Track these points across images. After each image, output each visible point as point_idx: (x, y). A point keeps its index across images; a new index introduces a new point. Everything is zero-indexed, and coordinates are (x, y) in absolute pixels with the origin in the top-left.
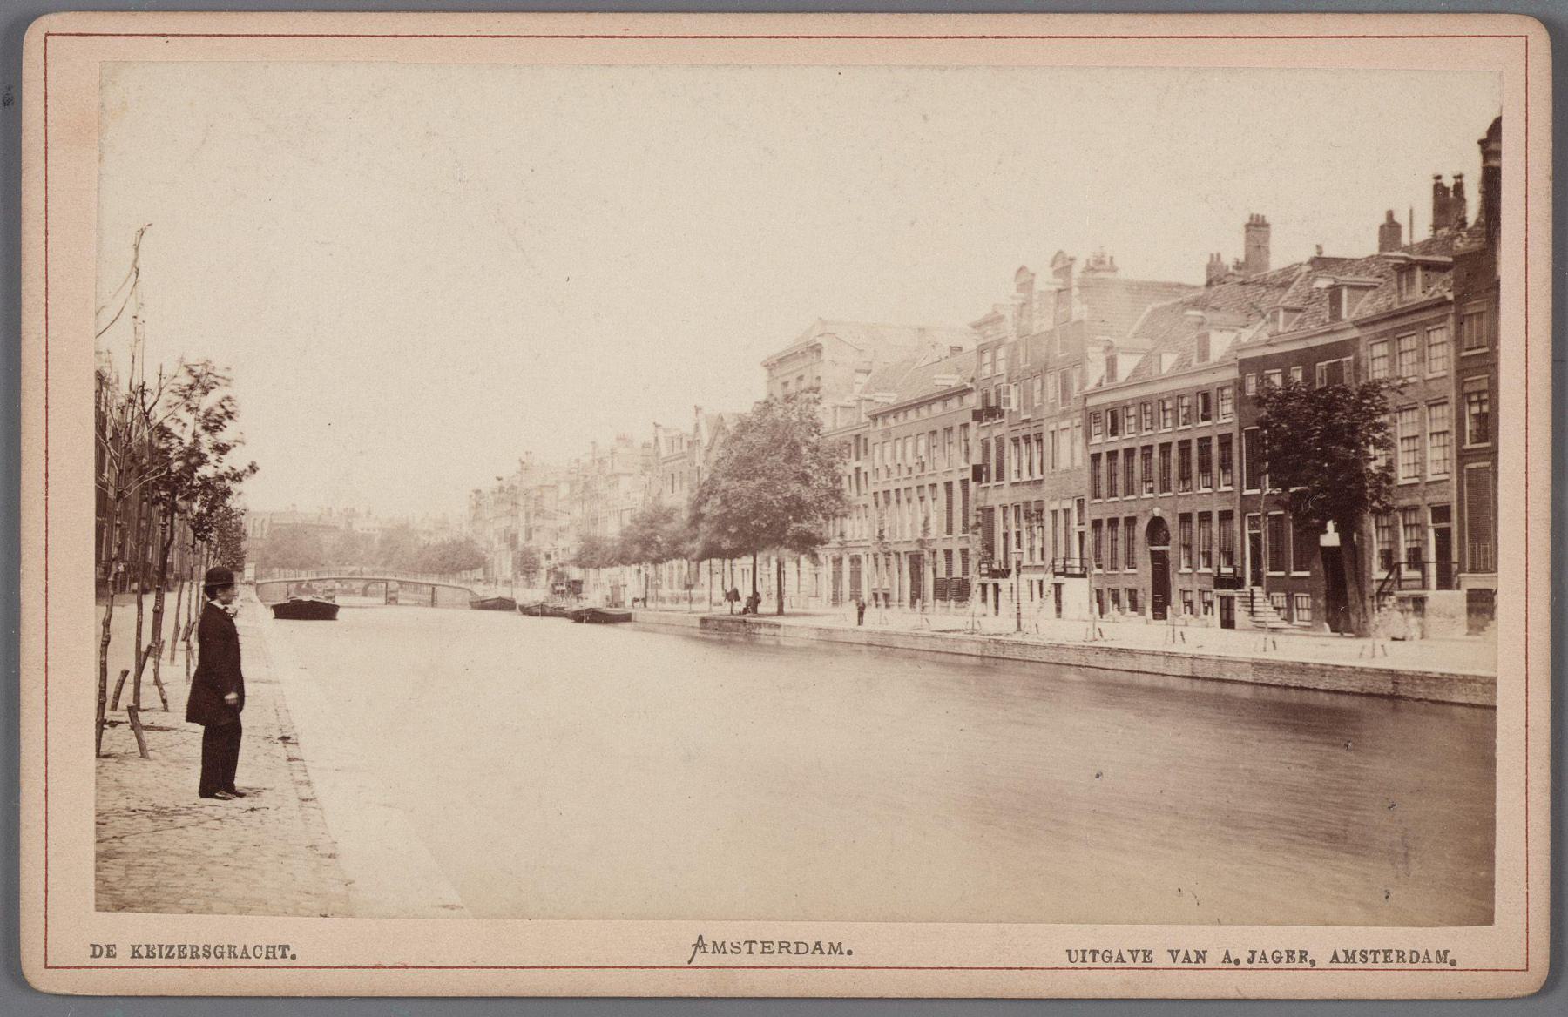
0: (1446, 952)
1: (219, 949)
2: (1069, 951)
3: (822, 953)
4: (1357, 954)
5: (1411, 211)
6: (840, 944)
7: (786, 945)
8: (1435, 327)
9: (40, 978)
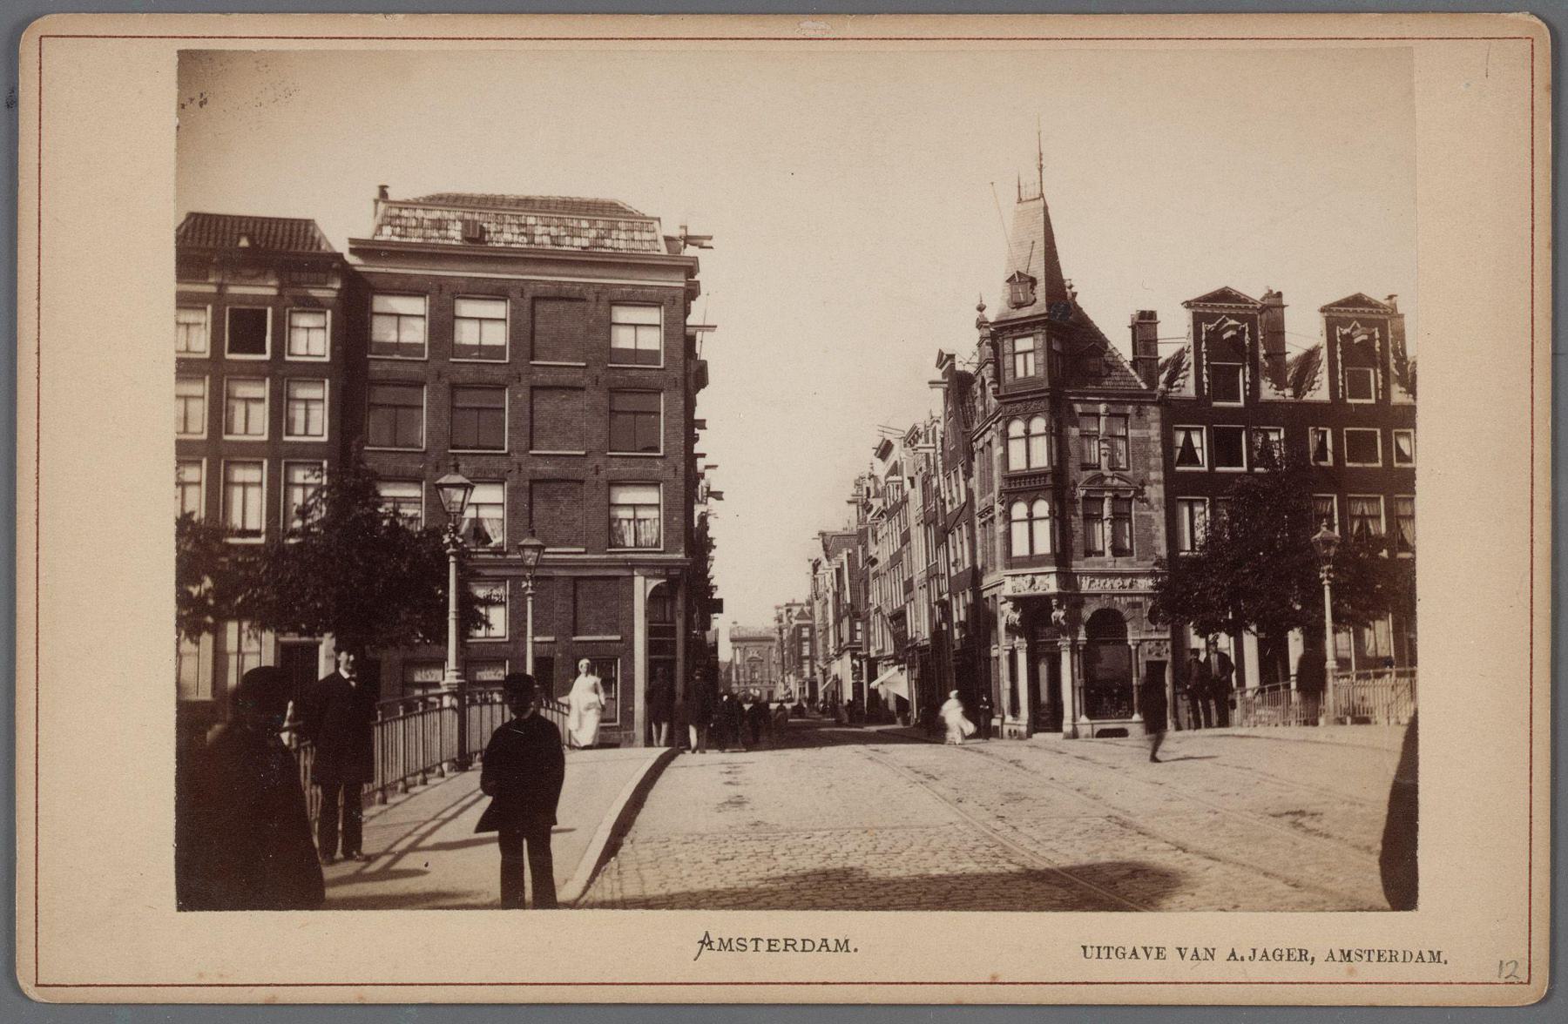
5: (1078, 757)
7: (792, 942)
9: (25, 981)
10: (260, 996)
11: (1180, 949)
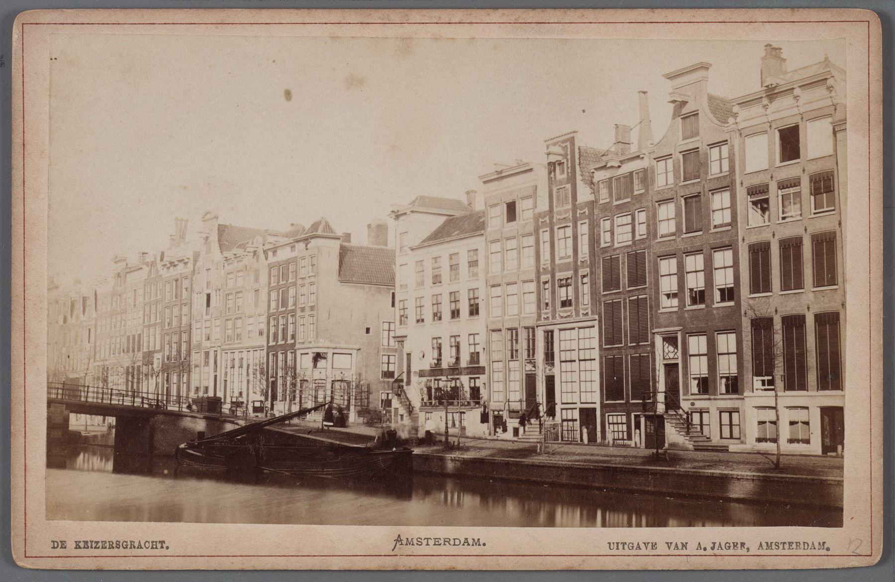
2: (609, 543)
3: (815, 549)
4: (773, 544)
6: (479, 539)
10: (237, 564)
11: (609, 543)
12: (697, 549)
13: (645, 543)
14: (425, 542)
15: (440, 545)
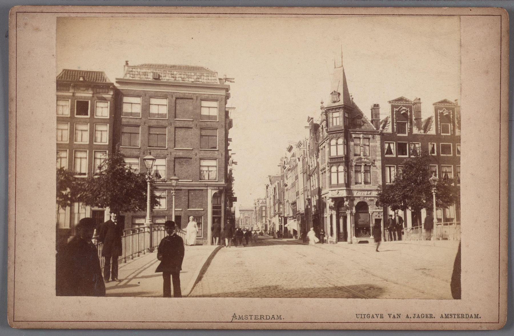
0: (478, 315)
1: (423, 315)
2: (357, 314)
3: (472, 318)
4: (449, 315)
6: (280, 316)
8: (282, 197)
12: (441, 318)
13: (376, 315)
14: (453, 316)
15: (258, 319)
